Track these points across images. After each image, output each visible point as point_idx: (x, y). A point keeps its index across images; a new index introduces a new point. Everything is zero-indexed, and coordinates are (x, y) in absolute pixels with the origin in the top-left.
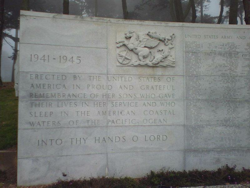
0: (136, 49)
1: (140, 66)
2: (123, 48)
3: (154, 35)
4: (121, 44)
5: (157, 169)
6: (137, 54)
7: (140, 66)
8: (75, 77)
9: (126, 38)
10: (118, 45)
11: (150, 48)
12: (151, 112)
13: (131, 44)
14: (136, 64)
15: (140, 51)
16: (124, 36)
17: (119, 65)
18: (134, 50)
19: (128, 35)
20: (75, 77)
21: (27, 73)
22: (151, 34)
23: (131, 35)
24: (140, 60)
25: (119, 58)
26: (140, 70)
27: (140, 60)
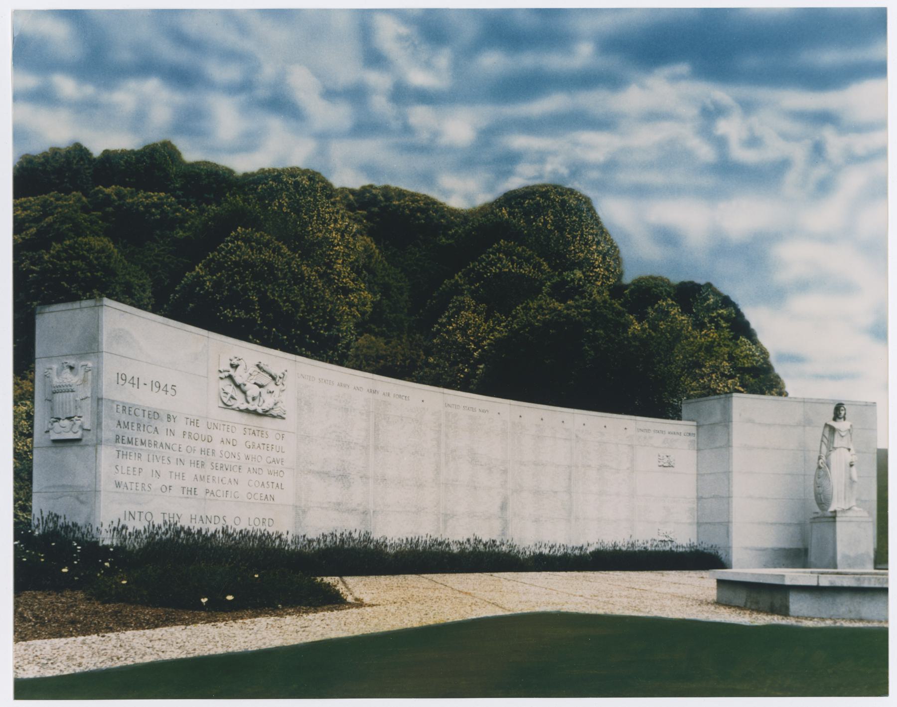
0: (245, 385)
1: (247, 411)
2: (228, 382)
3: (265, 368)
4: (227, 374)
5: (655, 274)
6: (244, 393)
7: (247, 411)
8: (169, 417)
9: (232, 365)
10: (222, 375)
11: (261, 386)
12: (257, 484)
13: (240, 376)
14: (243, 407)
15: (136, 426)
16: (229, 362)
17: (223, 405)
18: (242, 386)
19: (235, 362)
20: (169, 417)
21: (113, 401)
22: (262, 365)
23: (239, 362)
24: (248, 402)
25: (223, 395)
26: (245, 418)
27: (248, 402)
